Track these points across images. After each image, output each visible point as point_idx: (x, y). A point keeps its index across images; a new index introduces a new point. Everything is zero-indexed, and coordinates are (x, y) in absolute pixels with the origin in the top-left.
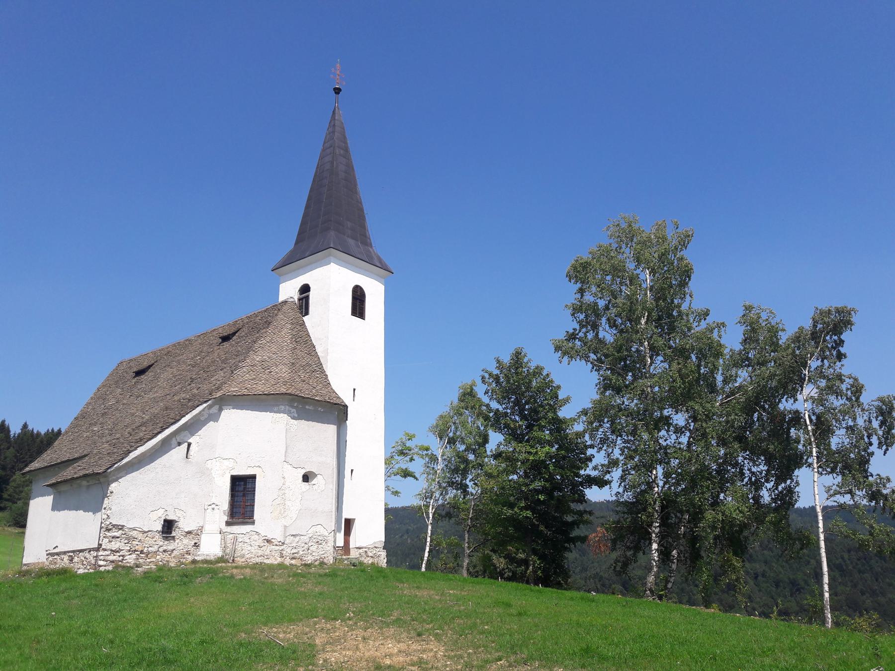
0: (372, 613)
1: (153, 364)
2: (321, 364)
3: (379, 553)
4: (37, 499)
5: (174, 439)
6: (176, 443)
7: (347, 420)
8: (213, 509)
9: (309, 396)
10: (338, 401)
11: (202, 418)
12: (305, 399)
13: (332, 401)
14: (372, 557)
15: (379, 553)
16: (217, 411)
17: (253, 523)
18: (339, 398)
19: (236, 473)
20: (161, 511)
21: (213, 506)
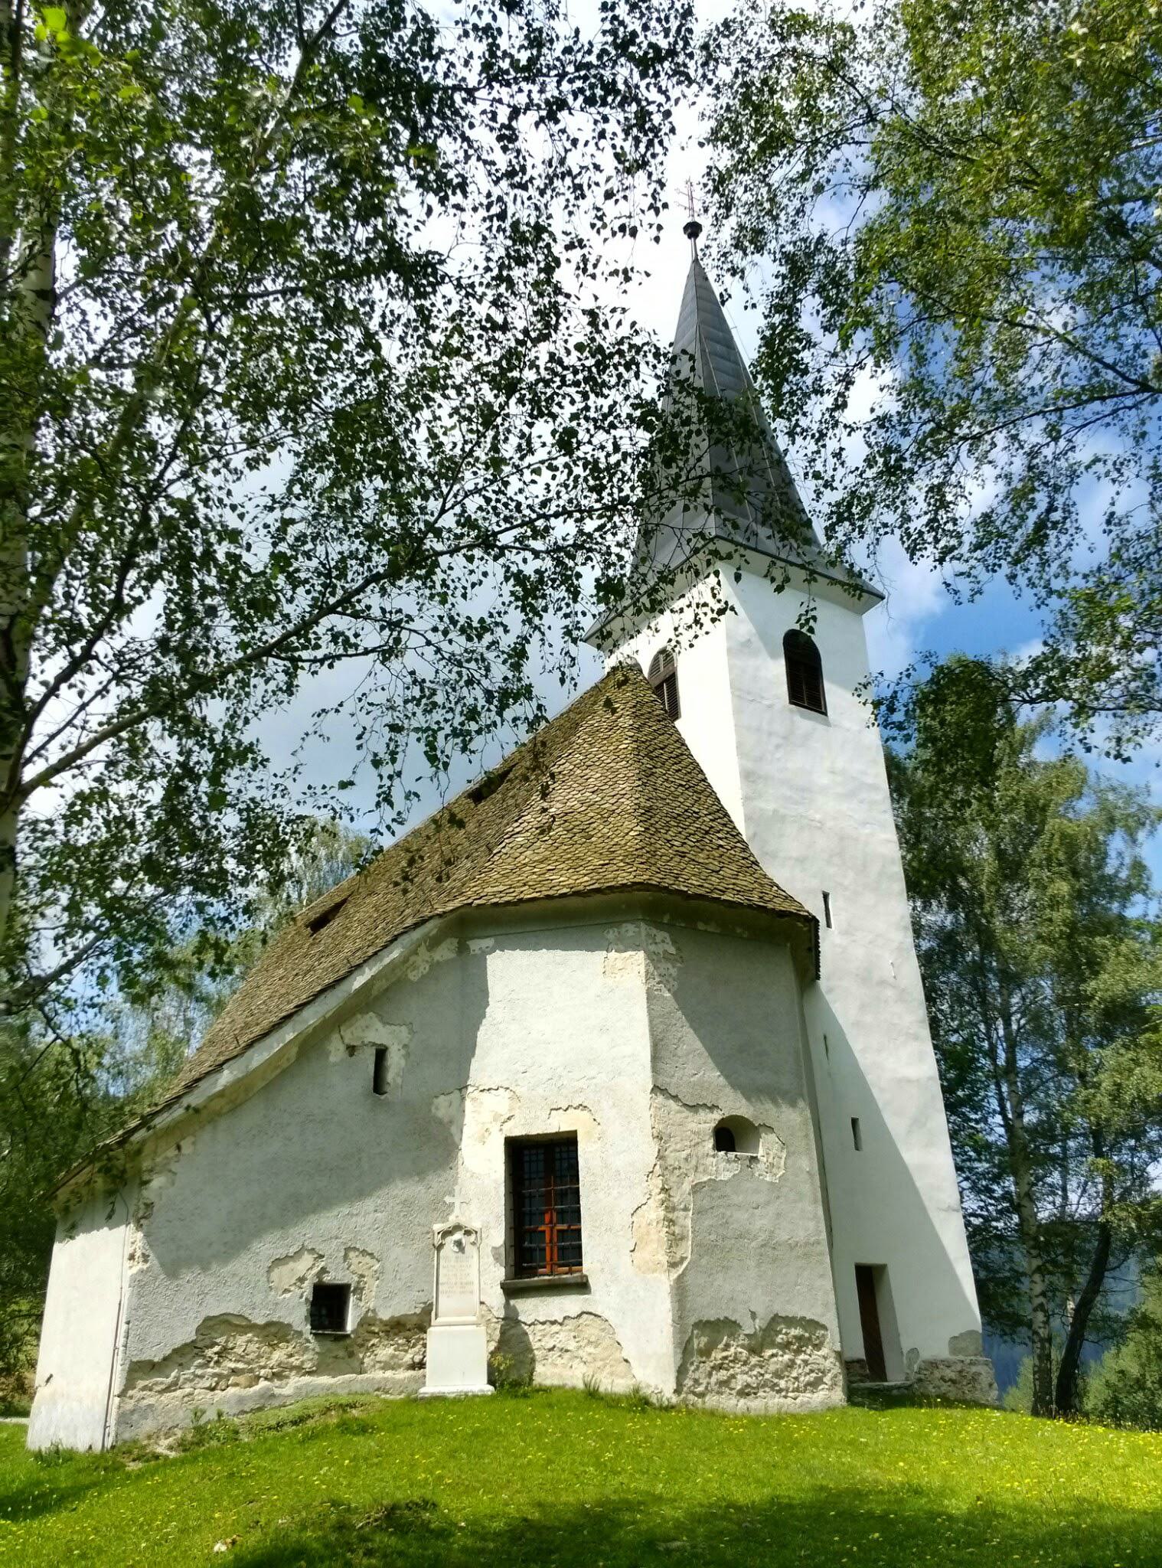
0: (267, 121)
1: (985, 1406)
2: (726, 815)
3: (974, 1369)
4: (83, 1241)
5: (335, 1037)
6: (342, 1048)
7: (818, 977)
8: (459, 1243)
9: (701, 891)
10: (786, 906)
11: (413, 976)
12: (693, 903)
13: (770, 906)
14: (953, 1382)
15: (974, 1369)
16: (453, 955)
17: (582, 1286)
18: (788, 898)
19: (517, 1130)
20: (307, 1260)
21: (458, 1236)
